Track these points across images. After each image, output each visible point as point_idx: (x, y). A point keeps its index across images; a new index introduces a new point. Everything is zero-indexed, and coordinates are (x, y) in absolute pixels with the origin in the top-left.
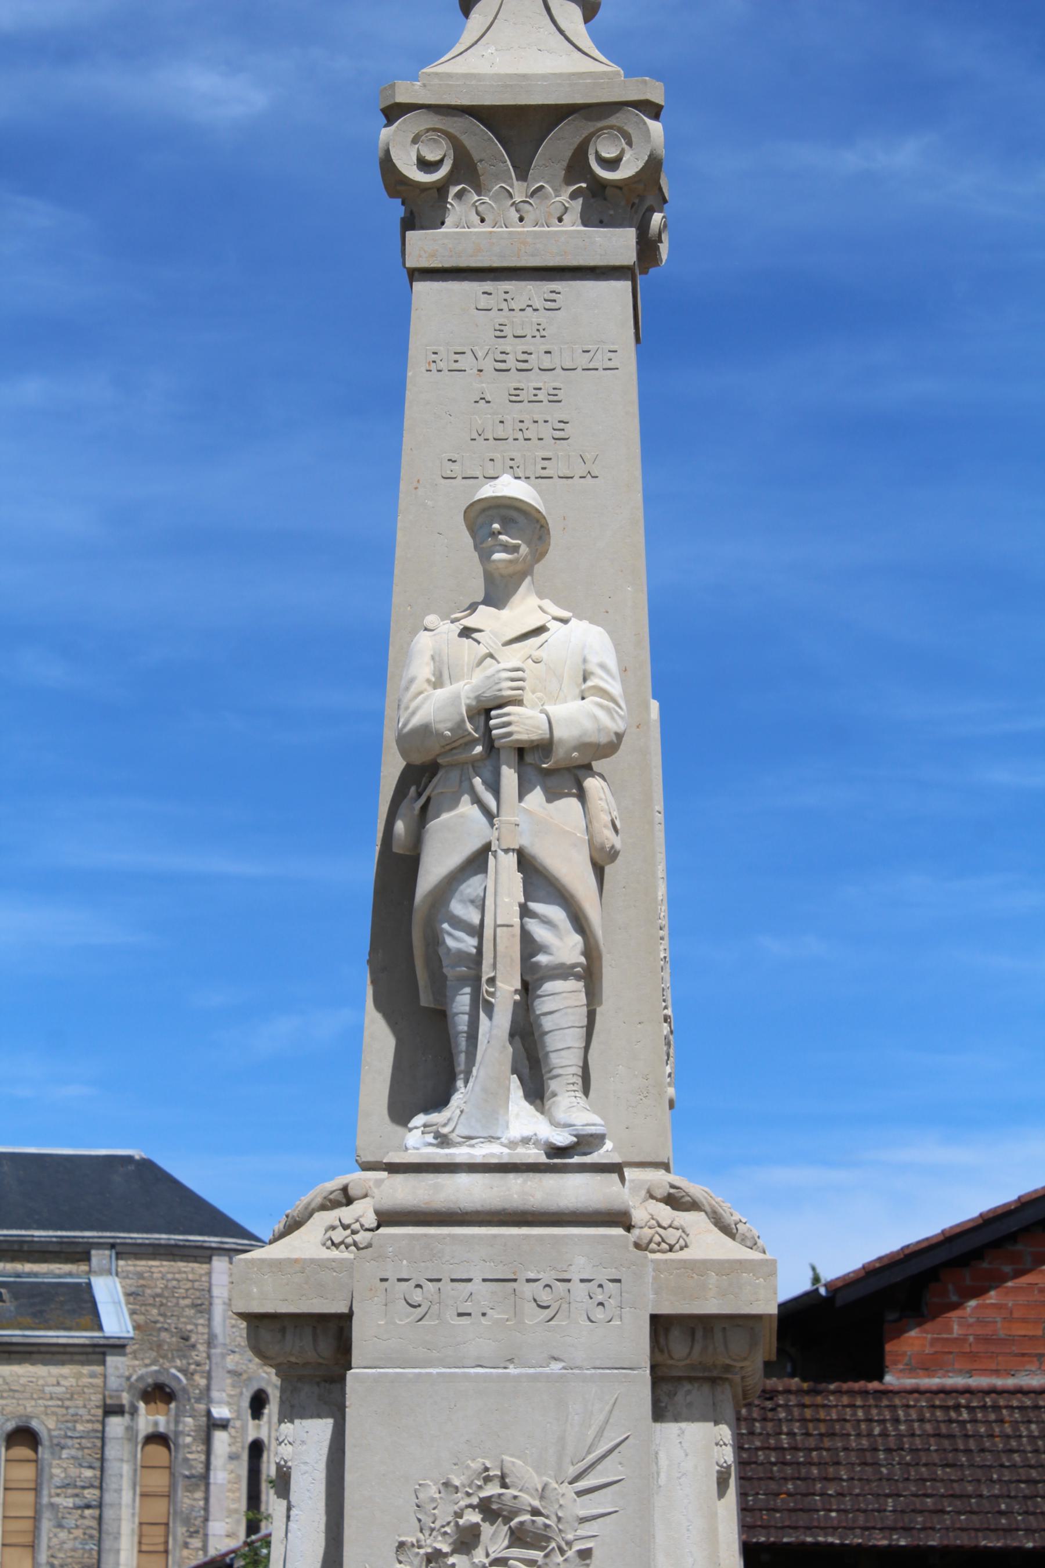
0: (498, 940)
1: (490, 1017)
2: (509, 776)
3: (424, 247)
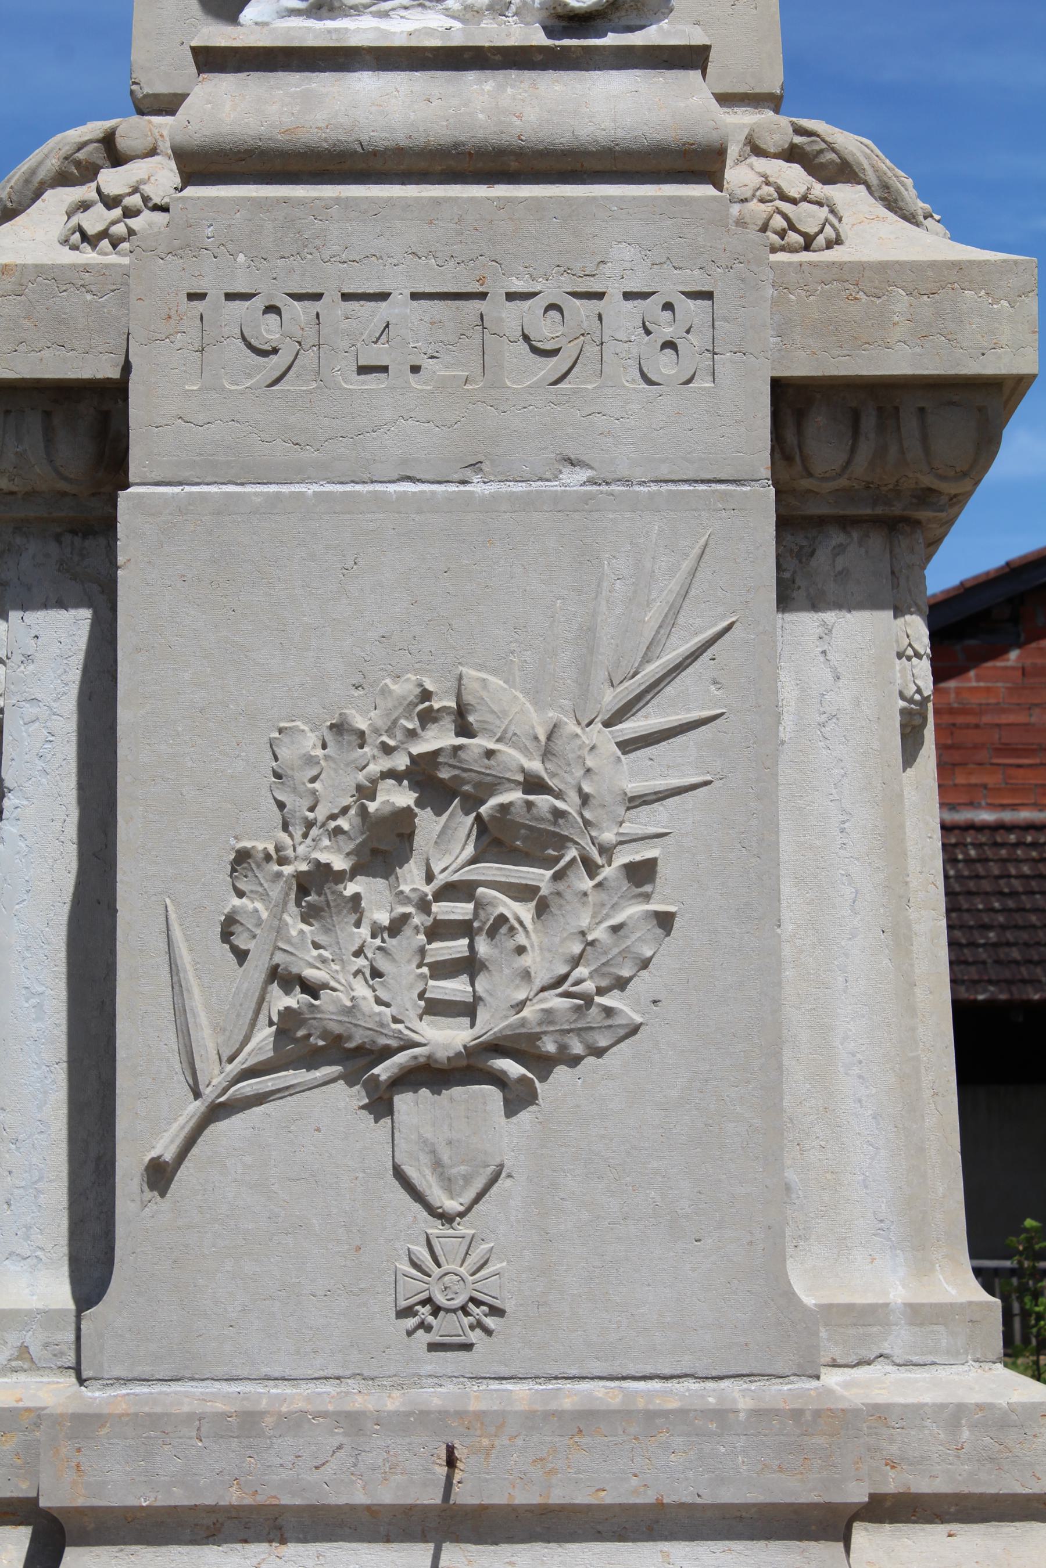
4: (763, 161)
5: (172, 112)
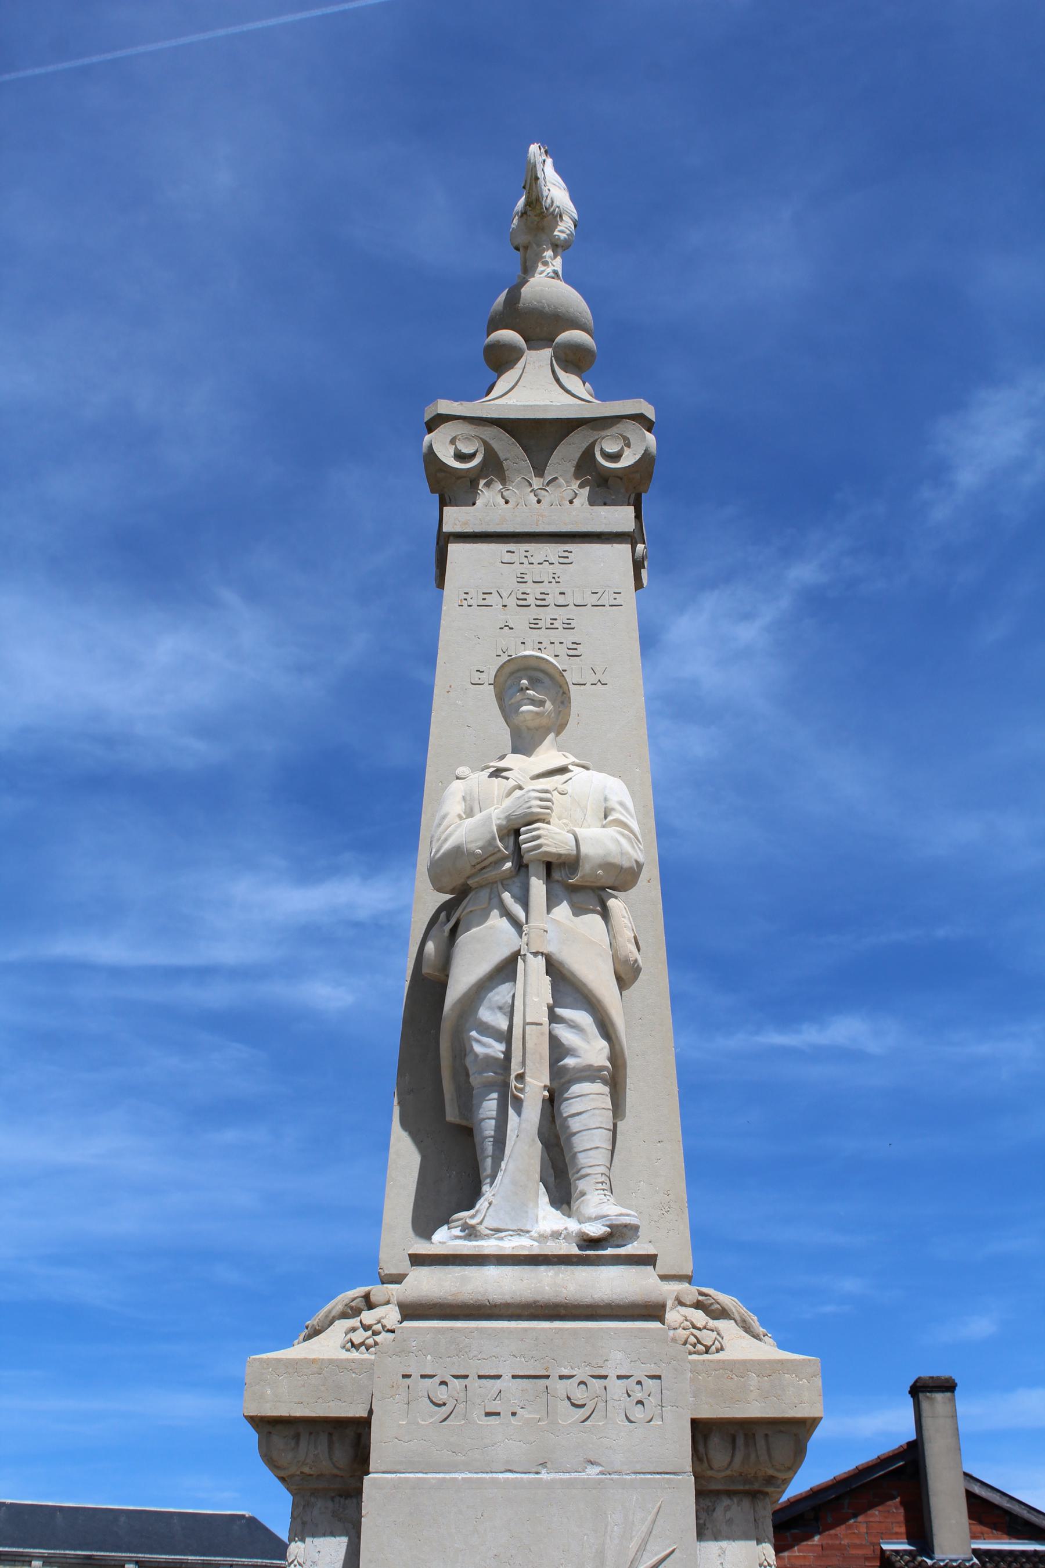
0: (527, 1037)
1: (519, 1114)
2: (538, 887)
3: (456, 518)
4: (684, 1308)
5: (399, 1282)
